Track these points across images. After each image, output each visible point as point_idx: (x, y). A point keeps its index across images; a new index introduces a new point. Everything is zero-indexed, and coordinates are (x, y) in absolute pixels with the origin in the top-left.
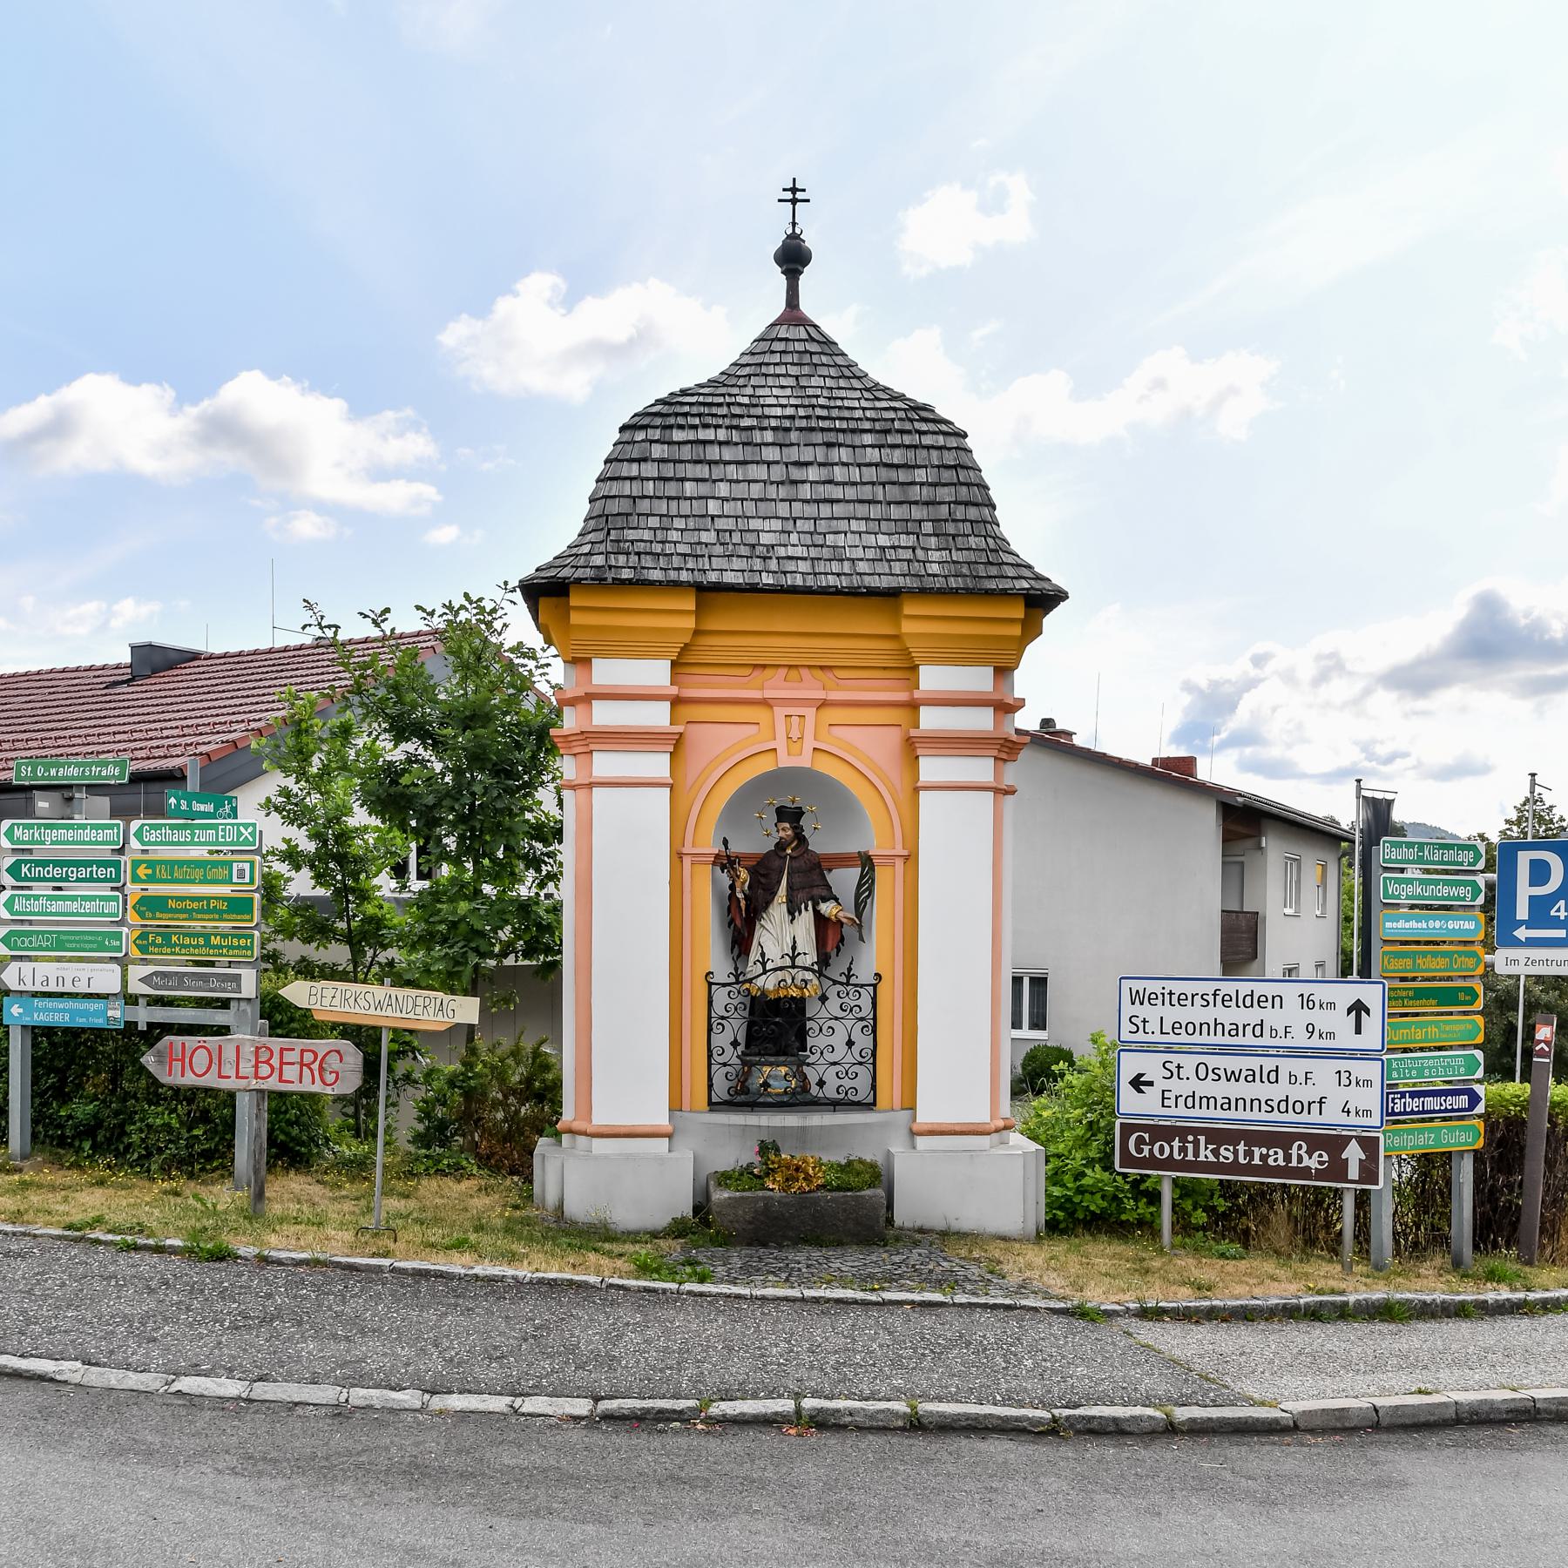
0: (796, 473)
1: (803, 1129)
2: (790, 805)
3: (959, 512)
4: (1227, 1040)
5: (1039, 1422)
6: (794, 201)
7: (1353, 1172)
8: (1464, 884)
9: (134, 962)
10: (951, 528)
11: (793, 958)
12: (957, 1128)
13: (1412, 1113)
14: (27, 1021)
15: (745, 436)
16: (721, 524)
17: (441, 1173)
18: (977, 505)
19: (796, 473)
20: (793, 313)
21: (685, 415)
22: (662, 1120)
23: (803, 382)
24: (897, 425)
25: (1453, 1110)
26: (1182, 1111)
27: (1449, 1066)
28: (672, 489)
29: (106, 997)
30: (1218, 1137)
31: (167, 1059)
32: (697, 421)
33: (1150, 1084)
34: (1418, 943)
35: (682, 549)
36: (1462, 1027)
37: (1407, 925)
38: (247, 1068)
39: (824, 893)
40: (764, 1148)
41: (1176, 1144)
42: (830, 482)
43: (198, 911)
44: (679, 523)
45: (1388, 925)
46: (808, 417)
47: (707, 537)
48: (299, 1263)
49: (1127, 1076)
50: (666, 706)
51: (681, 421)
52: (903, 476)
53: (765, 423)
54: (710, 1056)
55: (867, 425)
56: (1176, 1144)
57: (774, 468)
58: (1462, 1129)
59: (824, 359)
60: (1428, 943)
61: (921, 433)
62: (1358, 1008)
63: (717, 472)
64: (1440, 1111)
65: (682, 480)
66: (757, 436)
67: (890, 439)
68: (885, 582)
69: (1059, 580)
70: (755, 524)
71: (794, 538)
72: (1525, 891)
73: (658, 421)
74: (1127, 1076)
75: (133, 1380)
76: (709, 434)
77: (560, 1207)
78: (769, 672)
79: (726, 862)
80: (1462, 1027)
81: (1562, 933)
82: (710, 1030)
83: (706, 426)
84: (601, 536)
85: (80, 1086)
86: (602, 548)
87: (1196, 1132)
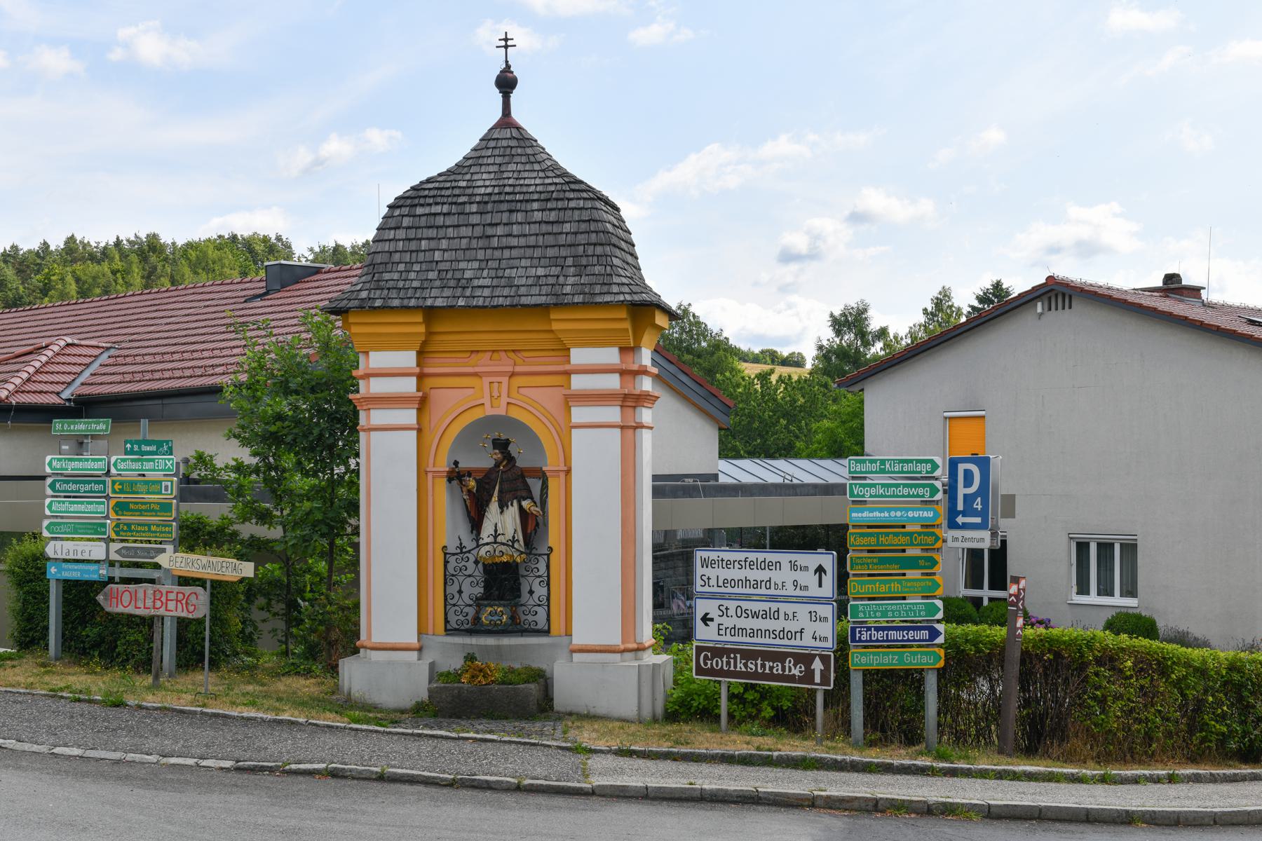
0: (490, 231)
1: (498, 647)
2: (503, 440)
3: (590, 250)
4: (752, 591)
5: (446, 779)
6: (506, 47)
7: (817, 679)
8: (924, 486)
9: (113, 541)
10: (584, 261)
11: (495, 537)
13: (877, 641)
14: (59, 576)
15: (460, 209)
16: (442, 266)
17: (298, 674)
18: (601, 244)
19: (490, 231)
20: (506, 120)
21: (425, 197)
22: (412, 639)
23: (503, 168)
24: (554, 195)
26: (728, 638)
28: (413, 245)
29: (98, 562)
30: (748, 655)
31: (109, 597)
32: (431, 201)
33: (712, 620)
35: (415, 284)
38: (149, 603)
39: (524, 494)
40: (470, 658)
41: (725, 659)
42: (510, 235)
43: (146, 511)
44: (417, 267)
45: (854, 515)
46: (500, 193)
47: (432, 275)
48: (156, 709)
49: (699, 615)
50: (414, 379)
51: (422, 201)
52: (556, 229)
53: (473, 199)
54: (446, 600)
55: (536, 197)
56: (725, 659)
57: (477, 228)
58: (926, 654)
59: (519, 151)
60: (869, 527)
61: (569, 199)
62: (820, 570)
63: (442, 233)
65: (420, 239)
66: (468, 209)
67: (549, 205)
68: (542, 300)
70: (462, 265)
71: (486, 272)
72: (962, 491)
73: (409, 202)
74: (699, 615)
75: (35, 748)
76: (437, 209)
77: (349, 694)
78: (481, 355)
79: (456, 475)
80: (923, 584)
81: (978, 520)
82: (445, 583)
83: (437, 204)
84: (369, 277)
85: (93, 617)
86: (368, 286)
87: (735, 651)
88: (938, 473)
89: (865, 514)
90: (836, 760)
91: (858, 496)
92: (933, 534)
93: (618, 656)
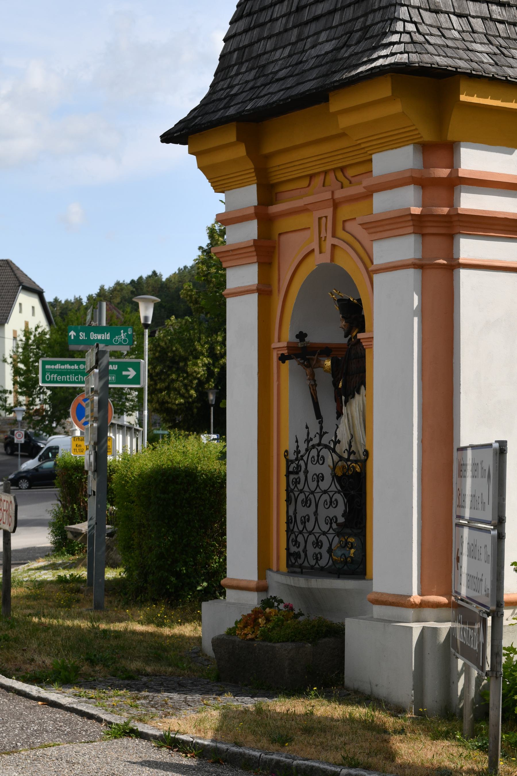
12: (390, 599)
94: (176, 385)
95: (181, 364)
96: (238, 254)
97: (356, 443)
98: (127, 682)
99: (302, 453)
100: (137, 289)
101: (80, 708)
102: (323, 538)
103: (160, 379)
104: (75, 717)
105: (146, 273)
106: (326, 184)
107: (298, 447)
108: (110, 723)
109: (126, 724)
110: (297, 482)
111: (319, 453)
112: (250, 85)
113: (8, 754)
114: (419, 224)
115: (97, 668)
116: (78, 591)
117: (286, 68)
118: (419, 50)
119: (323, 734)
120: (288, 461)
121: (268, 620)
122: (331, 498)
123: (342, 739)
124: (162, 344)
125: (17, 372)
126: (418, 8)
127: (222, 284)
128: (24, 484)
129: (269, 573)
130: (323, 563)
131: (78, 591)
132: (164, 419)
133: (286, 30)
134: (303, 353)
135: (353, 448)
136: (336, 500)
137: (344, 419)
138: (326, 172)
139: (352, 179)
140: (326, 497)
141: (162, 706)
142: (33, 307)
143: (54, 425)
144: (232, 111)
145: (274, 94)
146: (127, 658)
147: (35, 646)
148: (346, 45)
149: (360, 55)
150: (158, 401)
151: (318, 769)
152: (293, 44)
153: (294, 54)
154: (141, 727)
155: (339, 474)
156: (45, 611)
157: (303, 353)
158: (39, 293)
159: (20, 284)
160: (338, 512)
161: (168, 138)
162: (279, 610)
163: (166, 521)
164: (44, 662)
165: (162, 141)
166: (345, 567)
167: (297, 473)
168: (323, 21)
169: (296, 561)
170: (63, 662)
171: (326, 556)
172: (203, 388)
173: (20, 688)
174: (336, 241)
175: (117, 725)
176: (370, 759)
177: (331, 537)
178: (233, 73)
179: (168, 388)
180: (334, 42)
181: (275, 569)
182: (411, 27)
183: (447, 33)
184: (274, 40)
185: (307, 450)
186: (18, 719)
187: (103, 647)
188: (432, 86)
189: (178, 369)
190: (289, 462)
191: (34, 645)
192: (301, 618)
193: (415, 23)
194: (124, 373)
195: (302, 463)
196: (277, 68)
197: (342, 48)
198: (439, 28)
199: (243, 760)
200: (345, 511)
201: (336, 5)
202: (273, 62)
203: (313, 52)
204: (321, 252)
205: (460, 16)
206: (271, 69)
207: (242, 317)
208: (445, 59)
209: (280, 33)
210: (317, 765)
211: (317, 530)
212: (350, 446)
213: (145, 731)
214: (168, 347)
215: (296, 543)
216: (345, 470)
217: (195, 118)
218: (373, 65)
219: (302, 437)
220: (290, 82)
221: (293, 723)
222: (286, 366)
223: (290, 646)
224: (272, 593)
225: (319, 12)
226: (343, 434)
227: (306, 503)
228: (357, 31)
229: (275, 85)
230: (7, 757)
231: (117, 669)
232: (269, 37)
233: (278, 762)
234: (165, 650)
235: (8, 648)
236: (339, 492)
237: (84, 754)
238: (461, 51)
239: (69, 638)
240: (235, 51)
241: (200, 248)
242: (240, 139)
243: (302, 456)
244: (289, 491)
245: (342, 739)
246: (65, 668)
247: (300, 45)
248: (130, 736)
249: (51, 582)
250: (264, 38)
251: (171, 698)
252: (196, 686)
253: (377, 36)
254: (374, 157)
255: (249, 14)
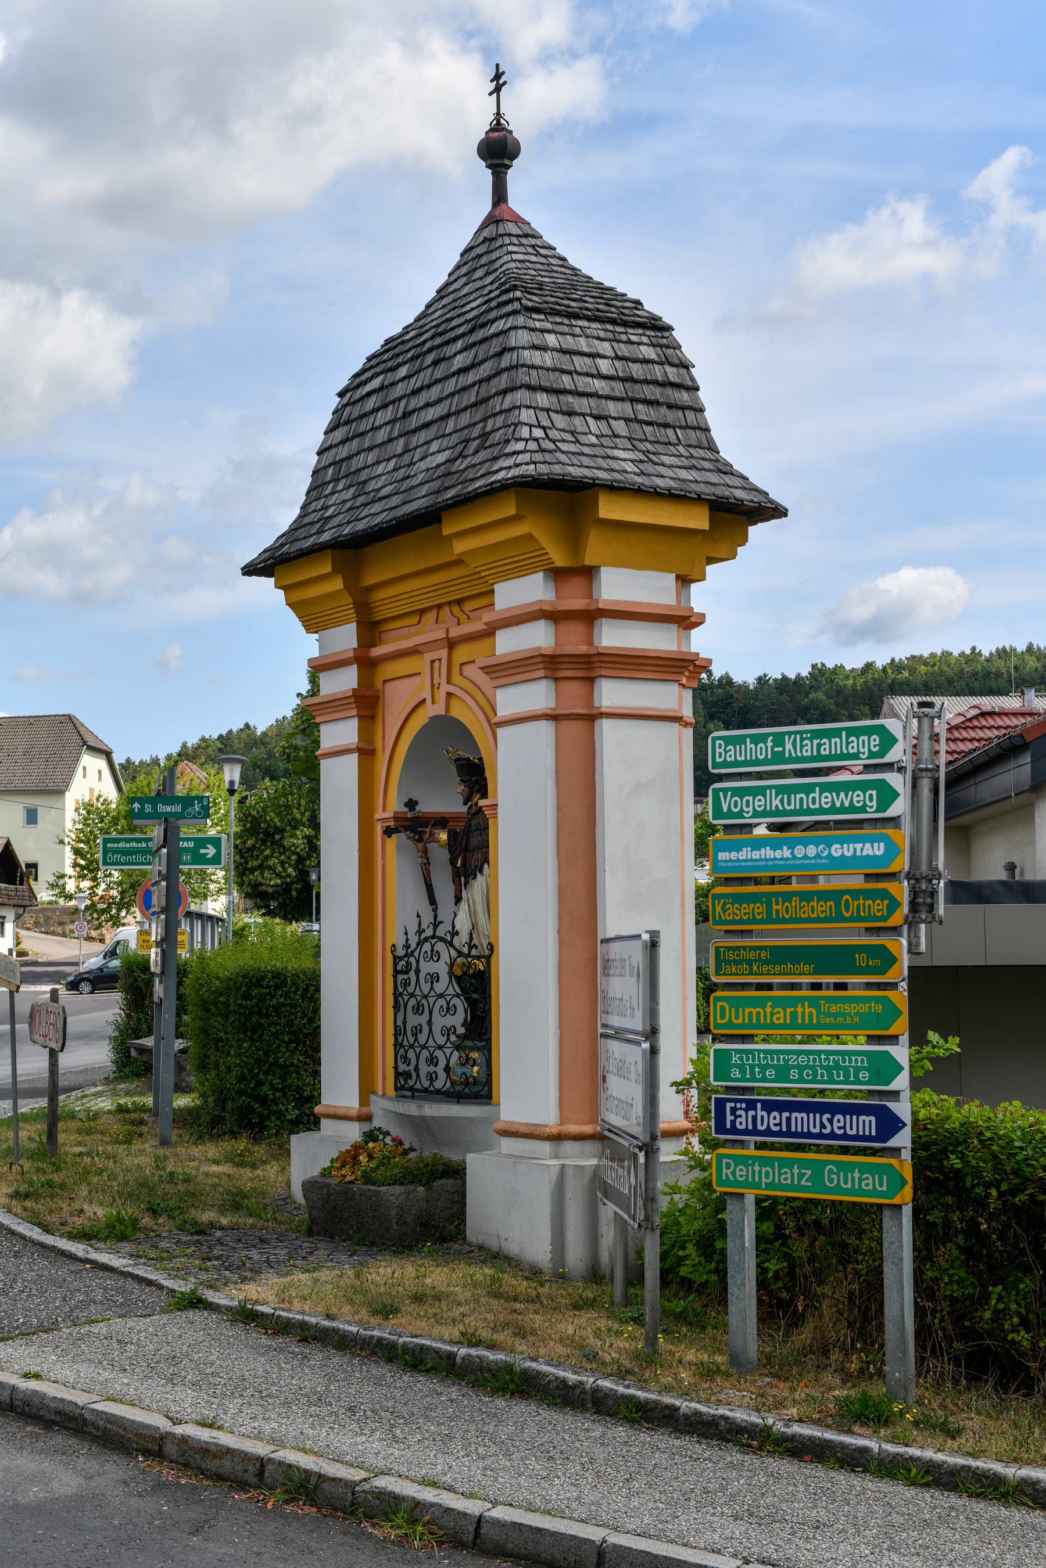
12: (522, 1130)
25: (845, 1137)
27: (837, 1066)
34: (757, 881)
36: (863, 1008)
37: (756, 855)
64: (820, 1136)
69: (778, 495)
80: (863, 1008)
88: (895, 754)
89: (745, 854)
90: (564, 1381)
91: (730, 815)
92: (885, 894)
93: (546, 1147)
94: (271, 863)
95: (277, 837)
96: (335, 706)
97: (478, 934)
98: (196, 1238)
99: (412, 948)
100: (225, 746)
101: (136, 1272)
102: (439, 1053)
103: (252, 856)
104: (130, 1284)
105: (236, 726)
106: (440, 620)
107: (407, 940)
108: (173, 1291)
109: (193, 1292)
110: (406, 984)
111: (433, 947)
112: (348, 505)
113: (46, 1332)
114: (550, 665)
115: (161, 1221)
116: (142, 1122)
117: (391, 484)
118: (548, 459)
119: (437, 1303)
120: (395, 957)
121: (371, 1157)
122: (448, 1004)
123: (461, 1310)
124: (254, 813)
125: (77, 852)
126: (548, 410)
127: (317, 743)
128: (85, 987)
129: (373, 1097)
130: (439, 1084)
131: (142, 1122)
132: (256, 904)
133: (390, 440)
134: (413, 825)
135: (475, 941)
136: (454, 1006)
137: (464, 905)
138: (439, 607)
139: (471, 615)
140: (442, 1002)
141: (239, 1268)
142: (100, 772)
143: (123, 914)
144: (326, 537)
145: (376, 515)
146: (198, 1207)
147: (86, 1193)
148: (462, 455)
149: (478, 467)
150: (250, 883)
151: (430, 1349)
152: (399, 455)
153: (401, 468)
154: (210, 1296)
155: (459, 973)
156: (100, 1148)
157: (413, 825)
158: (108, 755)
159: (85, 743)
160: (457, 1020)
161: (250, 570)
162: (385, 1144)
163: (249, 1034)
164: (95, 1214)
165: (244, 574)
166: (467, 1090)
167: (407, 972)
168: (434, 428)
169: (406, 1082)
170: (119, 1213)
171: (442, 1075)
172: (304, 865)
173: (64, 1248)
174: (452, 689)
175: (182, 1292)
176: (495, 1336)
177: (448, 1052)
178: (328, 492)
179: (261, 867)
180: (447, 452)
181: (380, 1093)
182: (538, 433)
183: (583, 439)
184: (376, 451)
185: (418, 944)
186: (60, 1287)
187: (169, 1193)
188: (566, 497)
189: (273, 843)
190: (396, 959)
191: (84, 1192)
192: (412, 1155)
193: (544, 428)
194: (202, 851)
195: (412, 959)
196: (380, 485)
197: (457, 459)
198: (572, 433)
199: (336, 1337)
200: (466, 1020)
201: (450, 409)
202: (375, 477)
203: (423, 465)
204: (433, 702)
205: (597, 418)
206: (372, 485)
207: (339, 781)
208: (580, 469)
209: (383, 444)
210: (428, 1343)
211: (431, 1043)
212: (471, 939)
213: (216, 1300)
214: (261, 817)
215: (406, 1060)
216: (465, 969)
217: (282, 545)
218: (494, 478)
219: (413, 929)
220: (395, 500)
221: (400, 1289)
222: (392, 842)
223: (397, 1190)
224: (377, 1123)
225: (429, 418)
226: (463, 923)
227: (418, 1009)
228: (475, 439)
229: (377, 505)
230: (44, 1336)
231: (185, 1222)
232: (370, 449)
233: (380, 1340)
234: (244, 1196)
235: (52, 1196)
236: (458, 995)
237: (139, 1332)
238: (600, 460)
239: (127, 1183)
240: (330, 465)
241: (299, 695)
242: (336, 570)
243: (413, 952)
244: (396, 995)
245: (461, 1310)
246: (121, 1221)
247: (407, 458)
248: (196, 1307)
249: (109, 1112)
250: (364, 450)
251: (250, 1258)
252: (282, 1242)
253: (498, 444)
254: (496, 586)
255: (347, 423)
